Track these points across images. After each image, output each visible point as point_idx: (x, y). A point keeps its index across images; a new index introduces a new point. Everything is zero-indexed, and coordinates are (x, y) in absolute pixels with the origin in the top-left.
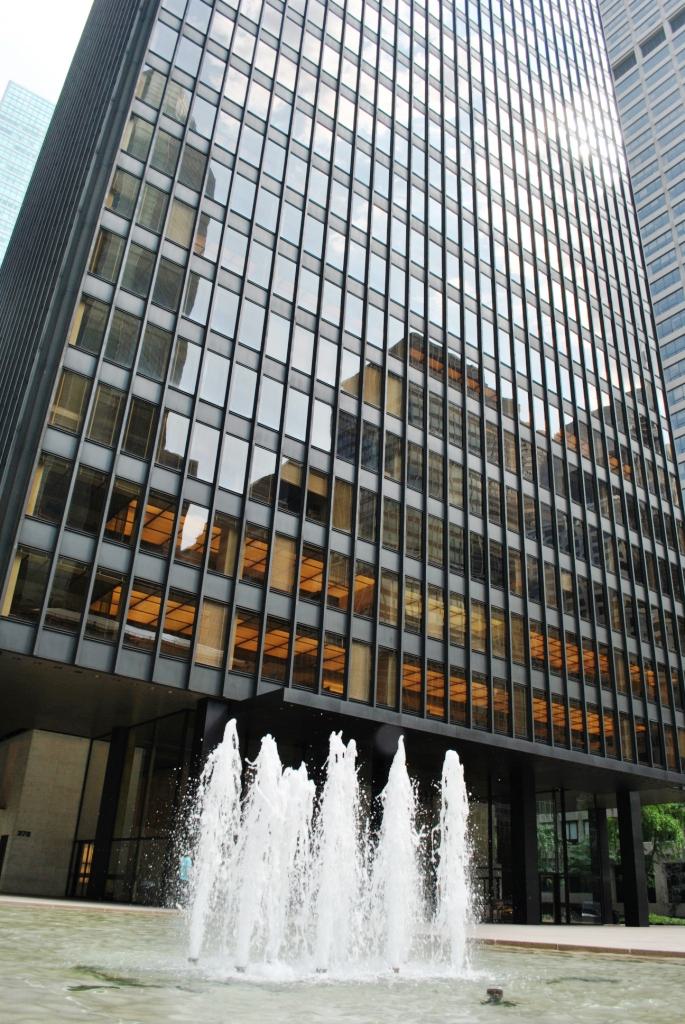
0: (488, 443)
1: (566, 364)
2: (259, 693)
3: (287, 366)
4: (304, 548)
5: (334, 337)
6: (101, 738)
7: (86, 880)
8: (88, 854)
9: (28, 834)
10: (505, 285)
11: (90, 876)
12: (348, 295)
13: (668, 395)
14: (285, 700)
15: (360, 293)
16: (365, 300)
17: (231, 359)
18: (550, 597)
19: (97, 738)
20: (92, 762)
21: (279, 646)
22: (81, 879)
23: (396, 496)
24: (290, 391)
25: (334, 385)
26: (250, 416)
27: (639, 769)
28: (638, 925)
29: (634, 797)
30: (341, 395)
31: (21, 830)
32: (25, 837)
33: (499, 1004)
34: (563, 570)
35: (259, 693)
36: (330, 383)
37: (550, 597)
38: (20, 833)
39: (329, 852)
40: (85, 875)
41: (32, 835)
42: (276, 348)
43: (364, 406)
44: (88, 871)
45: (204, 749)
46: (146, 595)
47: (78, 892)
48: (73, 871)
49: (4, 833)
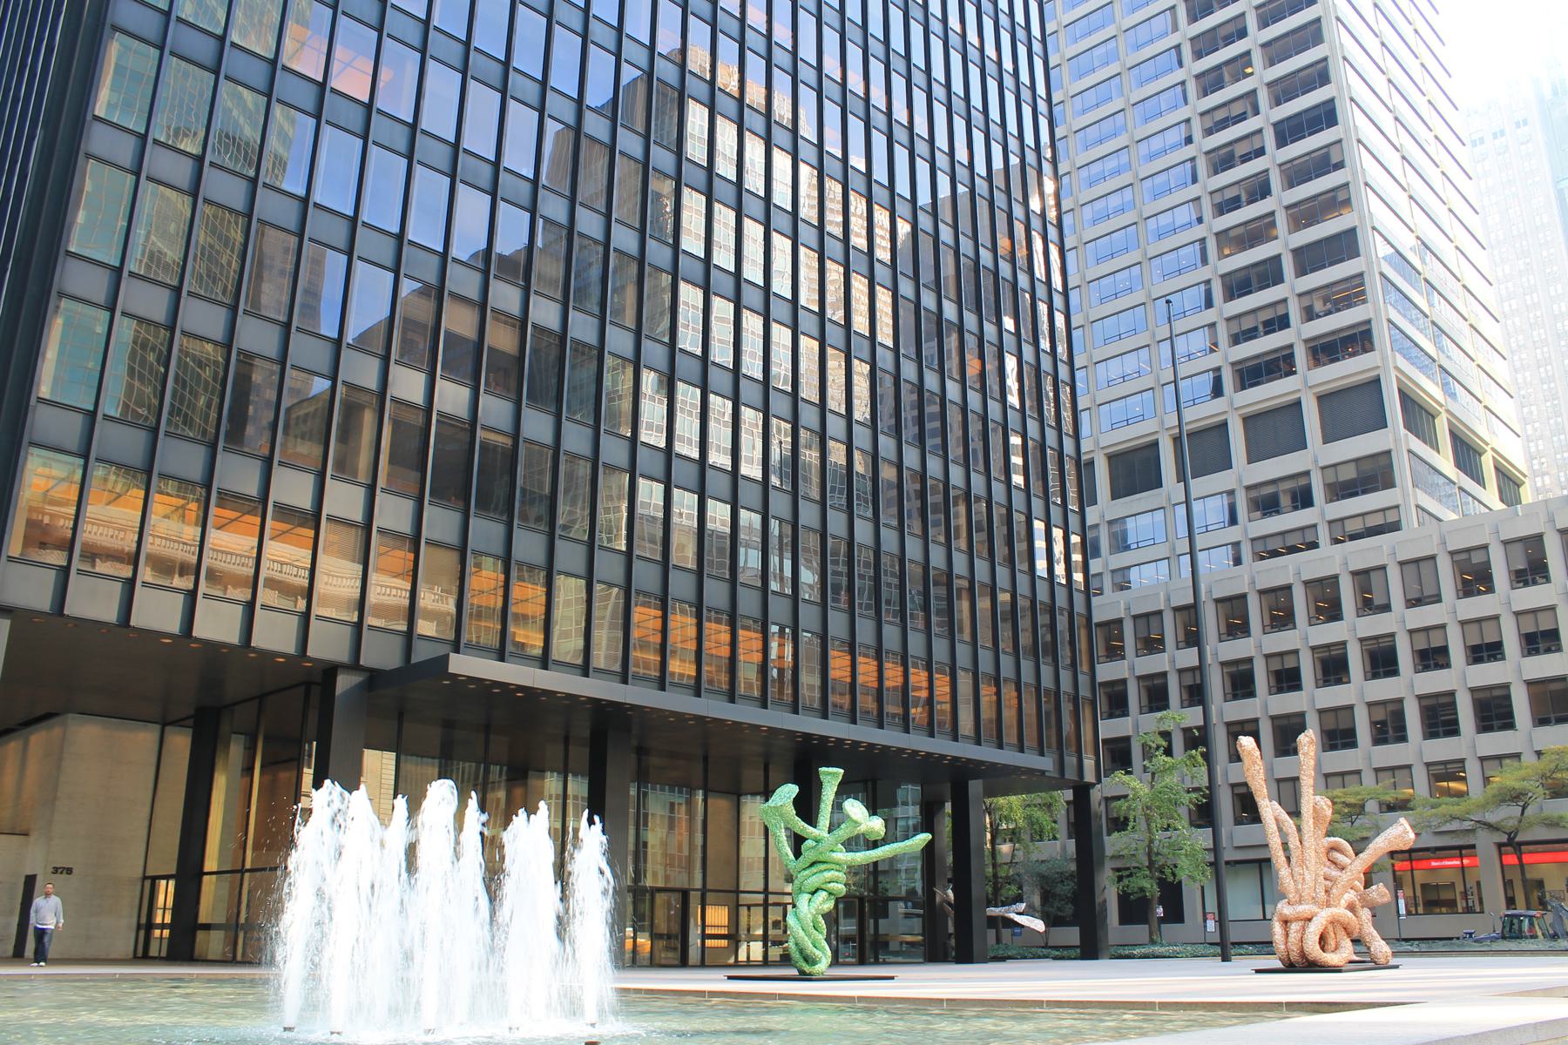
1: (859, 38)
2: (415, 659)
3: (413, 127)
4: (438, 421)
5: (533, 98)
7: (166, 933)
8: (166, 893)
9: (69, 871)
10: (814, 10)
11: (171, 926)
12: (557, 28)
13: (1053, 73)
14: (450, 671)
15: (577, 25)
16: (585, 36)
17: (365, 137)
18: (1001, 515)
19: (172, 723)
22: (157, 932)
23: (591, 338)
24: (419, 170)
25: (531, 176)
26: (395, 229)
27: (986, 753)
28: (971, 962)
29: (975, 787)
30: (541, 192)
32: (64, 876)
34: (884, 459)
35: (415, 659)
36: (524, 173)
37: (1001, 515)
38: (56, 870)
40: (163, 926)
42: (438, 119)
43: (579, 210)
44: (168, 920)
47: (153, 952)
48: (143, 921)
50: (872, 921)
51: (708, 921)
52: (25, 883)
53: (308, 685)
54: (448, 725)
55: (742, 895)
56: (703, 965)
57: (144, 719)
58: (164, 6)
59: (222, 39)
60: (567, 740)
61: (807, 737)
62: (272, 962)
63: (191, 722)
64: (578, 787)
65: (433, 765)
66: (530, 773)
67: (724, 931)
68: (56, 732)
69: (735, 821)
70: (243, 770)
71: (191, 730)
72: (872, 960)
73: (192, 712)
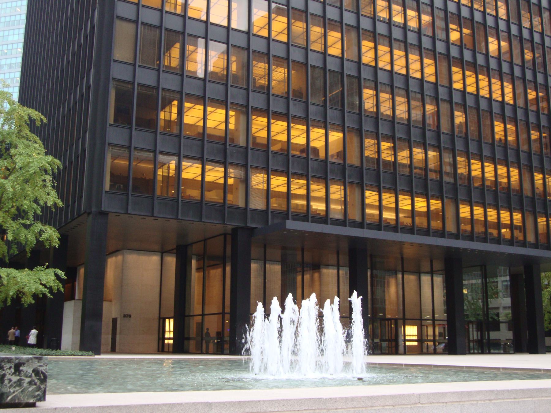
0: (338, 102)
6: (169, 252)
7: (171, 342)
8: (170, 325)
20: (163, 289)
21: (210, 170)
31: (126, 314)
32: (128, 318)
33: (346, 343)
38: (125, 316)
39: (329, 353)
40: (169, 339)
41: (132, 316)
44: (171, 335)
45: (252, 301)
46: (191, 164)
48: (161, 336)
49: (114, 316)
50: (486, 332)
51: (407, 333)
52: (113, 321)
53: (225, 235)
54: (284, 248)
55: (423, 321)
56: (405, 354)
57: (154, 251)
58: (158, 5)
59: (161, 11)
60: (303, 250)
61: (449, 248)
62: (248, 351)
63: (175, 251)
64: (344, 272)
65: (279, 265)
66: (321, 266)
67: (416, 338)
68: (120, 258)
69: (163, 282)
70: (196, 269)
71: (175, 255)
72: (487, 351)
73: (175, 247)
